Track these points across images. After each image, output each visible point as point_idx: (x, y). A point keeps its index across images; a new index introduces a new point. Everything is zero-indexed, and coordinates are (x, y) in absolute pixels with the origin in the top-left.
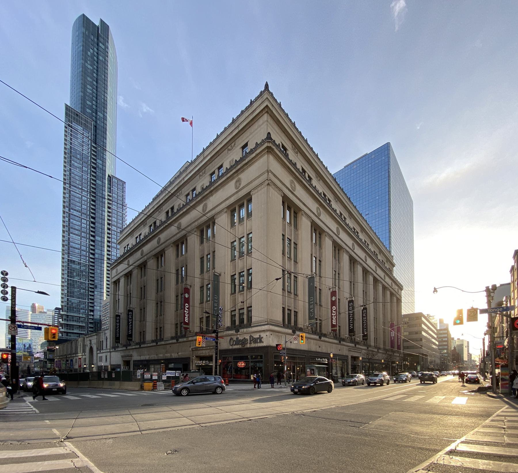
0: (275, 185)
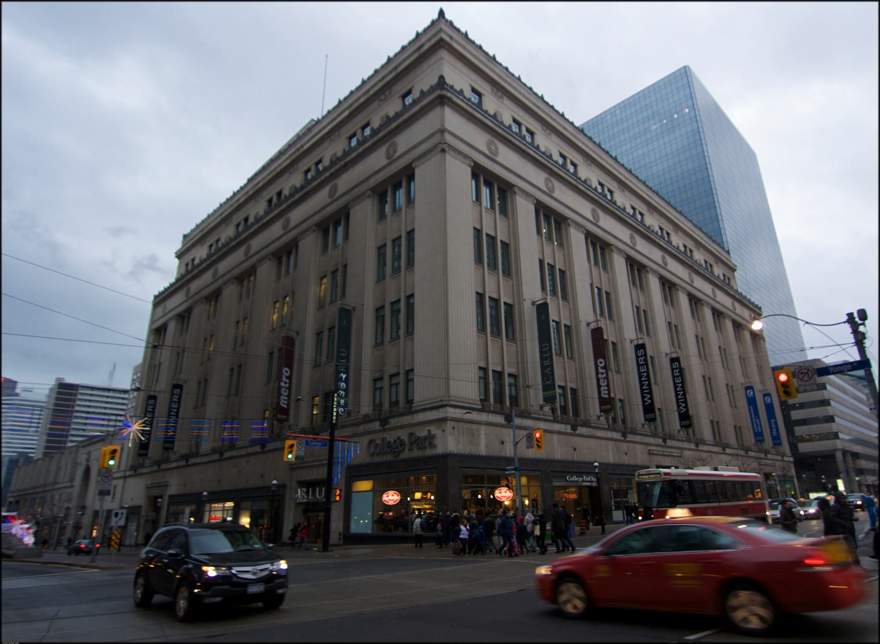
0: (455, 150)
